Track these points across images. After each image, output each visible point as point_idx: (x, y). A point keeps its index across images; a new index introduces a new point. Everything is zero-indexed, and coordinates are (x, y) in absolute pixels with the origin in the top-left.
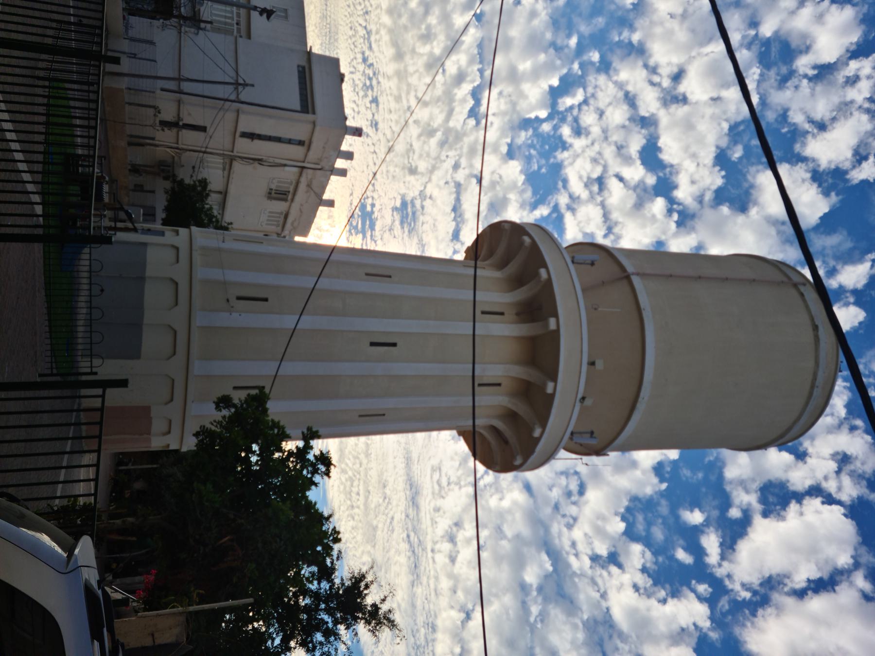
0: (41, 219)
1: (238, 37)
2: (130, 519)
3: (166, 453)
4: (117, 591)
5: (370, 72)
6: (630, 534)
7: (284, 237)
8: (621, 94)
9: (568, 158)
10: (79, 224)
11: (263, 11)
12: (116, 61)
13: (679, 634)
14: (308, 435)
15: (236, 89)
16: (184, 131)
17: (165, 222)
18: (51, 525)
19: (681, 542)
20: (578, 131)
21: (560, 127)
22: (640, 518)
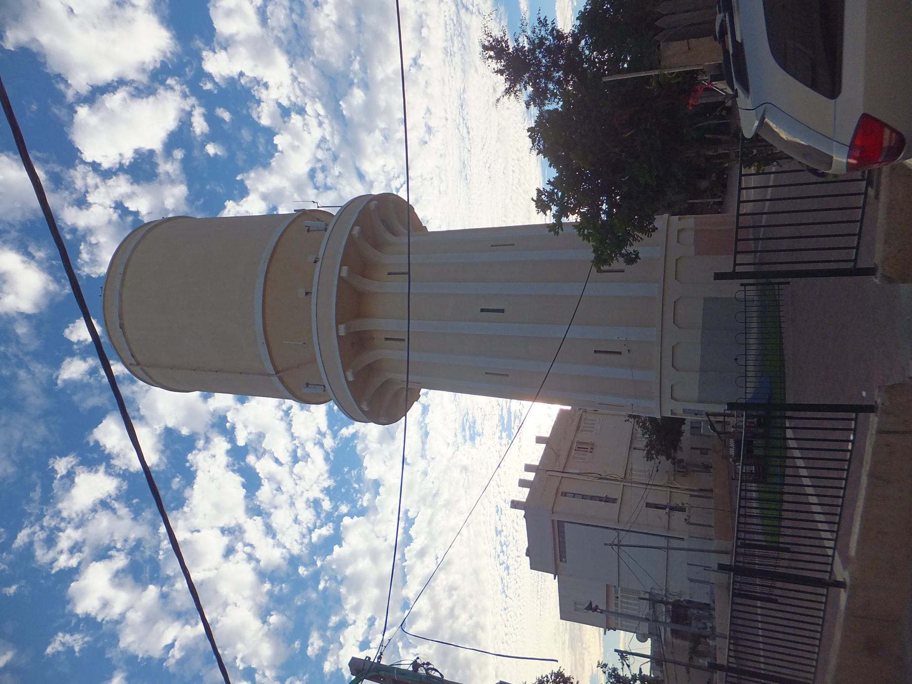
0: (788, 425)
1: (617, 586)
2: (711, 153)
3: (681, 213)
4: (722, 90)
5: (503, 558)
6: (270, 133)
7: (580, 409)
8: (279, 536)
9: (324, 480)
10: (755, 420)
11: (595, 609)
12: (722, 568)
13: (229, 45)
14: (558, 228)
15: (619, 541)
16: (665, 503)
17: (682, 421)
18: (779, 148)
19: (226, 127)
20: (316, 504)
21: (332, 508)
22: (261, 149)
